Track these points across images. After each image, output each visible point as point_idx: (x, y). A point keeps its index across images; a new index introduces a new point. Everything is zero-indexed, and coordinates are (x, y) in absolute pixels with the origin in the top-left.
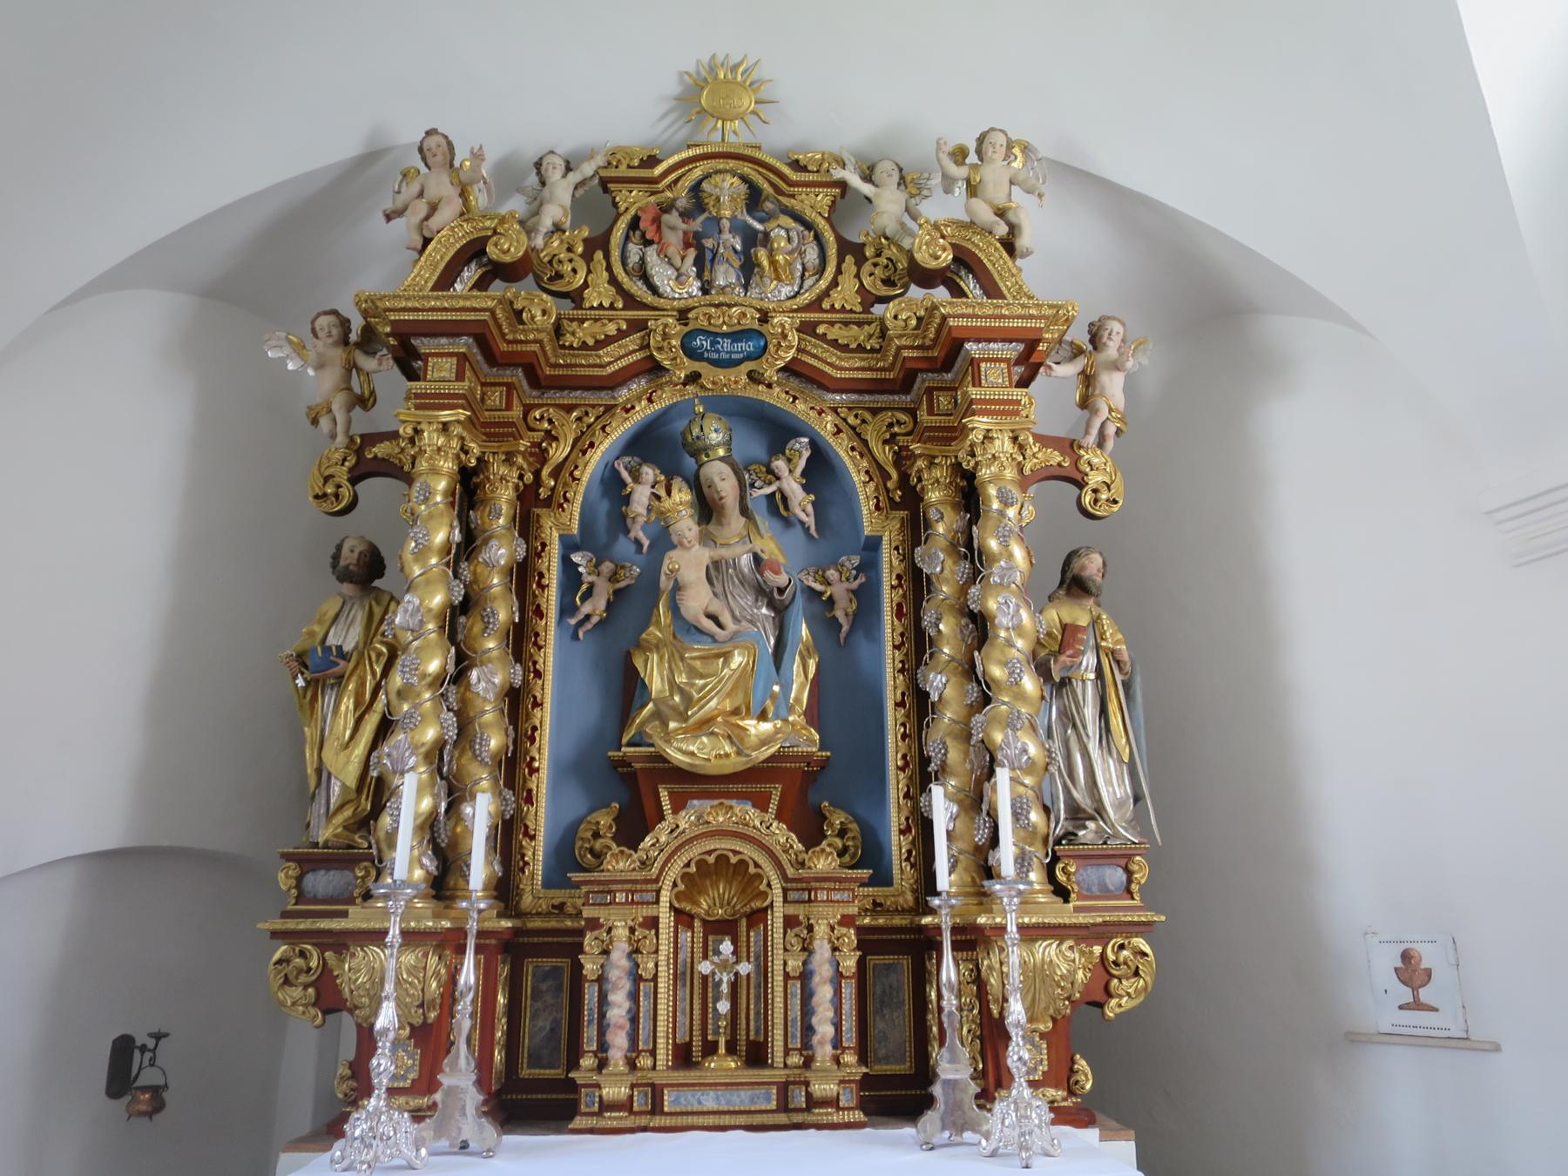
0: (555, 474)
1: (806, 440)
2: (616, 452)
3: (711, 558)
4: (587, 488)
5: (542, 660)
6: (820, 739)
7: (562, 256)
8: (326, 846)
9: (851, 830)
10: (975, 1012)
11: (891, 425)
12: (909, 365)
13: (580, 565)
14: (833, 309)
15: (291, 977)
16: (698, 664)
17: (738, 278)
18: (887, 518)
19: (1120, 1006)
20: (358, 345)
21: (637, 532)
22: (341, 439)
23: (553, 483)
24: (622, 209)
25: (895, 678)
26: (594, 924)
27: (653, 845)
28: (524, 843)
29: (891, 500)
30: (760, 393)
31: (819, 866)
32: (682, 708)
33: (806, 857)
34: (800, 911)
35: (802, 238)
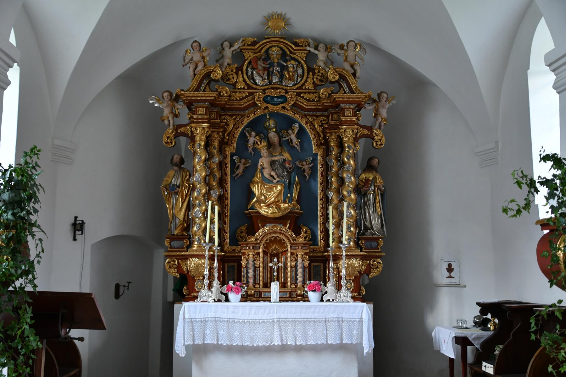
0: (228, 135)
7: (230, 73)
8: (177, 235)
10: (337, 276)
11: (321, 121)
14: (306, 89)
15: (171, 266)
17: (279, 80)
18: (319, 148)
19: (373, 275)
20: (174, 100)
21: (250, 150)
22: (171, 127)
24: (246, 58)
26: (244, 254)
29: (321, 143)
30: (285, 112)
33: (296, 238)
34: (295, 251)
35: (297, 66)
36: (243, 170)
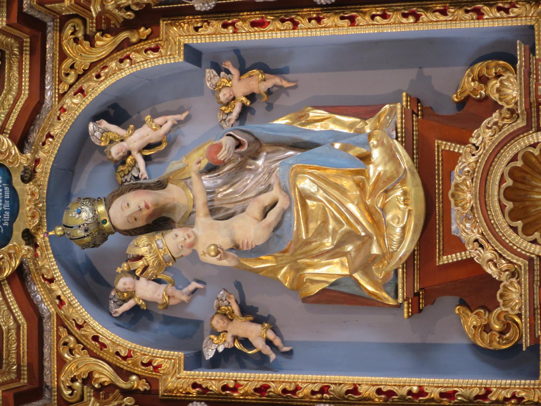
0: (125, 374)
1: (91, 126)
2: (105, 315)
3: (206, 215)
4: (137, 343)
5: (311, 385)
6: (390, 103)
9: (480, 71)
11: (76, 40)
12: (14, 20)
13: (217, 351)
16: (313, 226)
21: (181, 295)
23: (134, 377)
25: (325, 27)
27: (495, 265)
28: (494, 399)
29: (148, 37)
31: (515, 94)
32: (359, 243)
36: (254, 321)
